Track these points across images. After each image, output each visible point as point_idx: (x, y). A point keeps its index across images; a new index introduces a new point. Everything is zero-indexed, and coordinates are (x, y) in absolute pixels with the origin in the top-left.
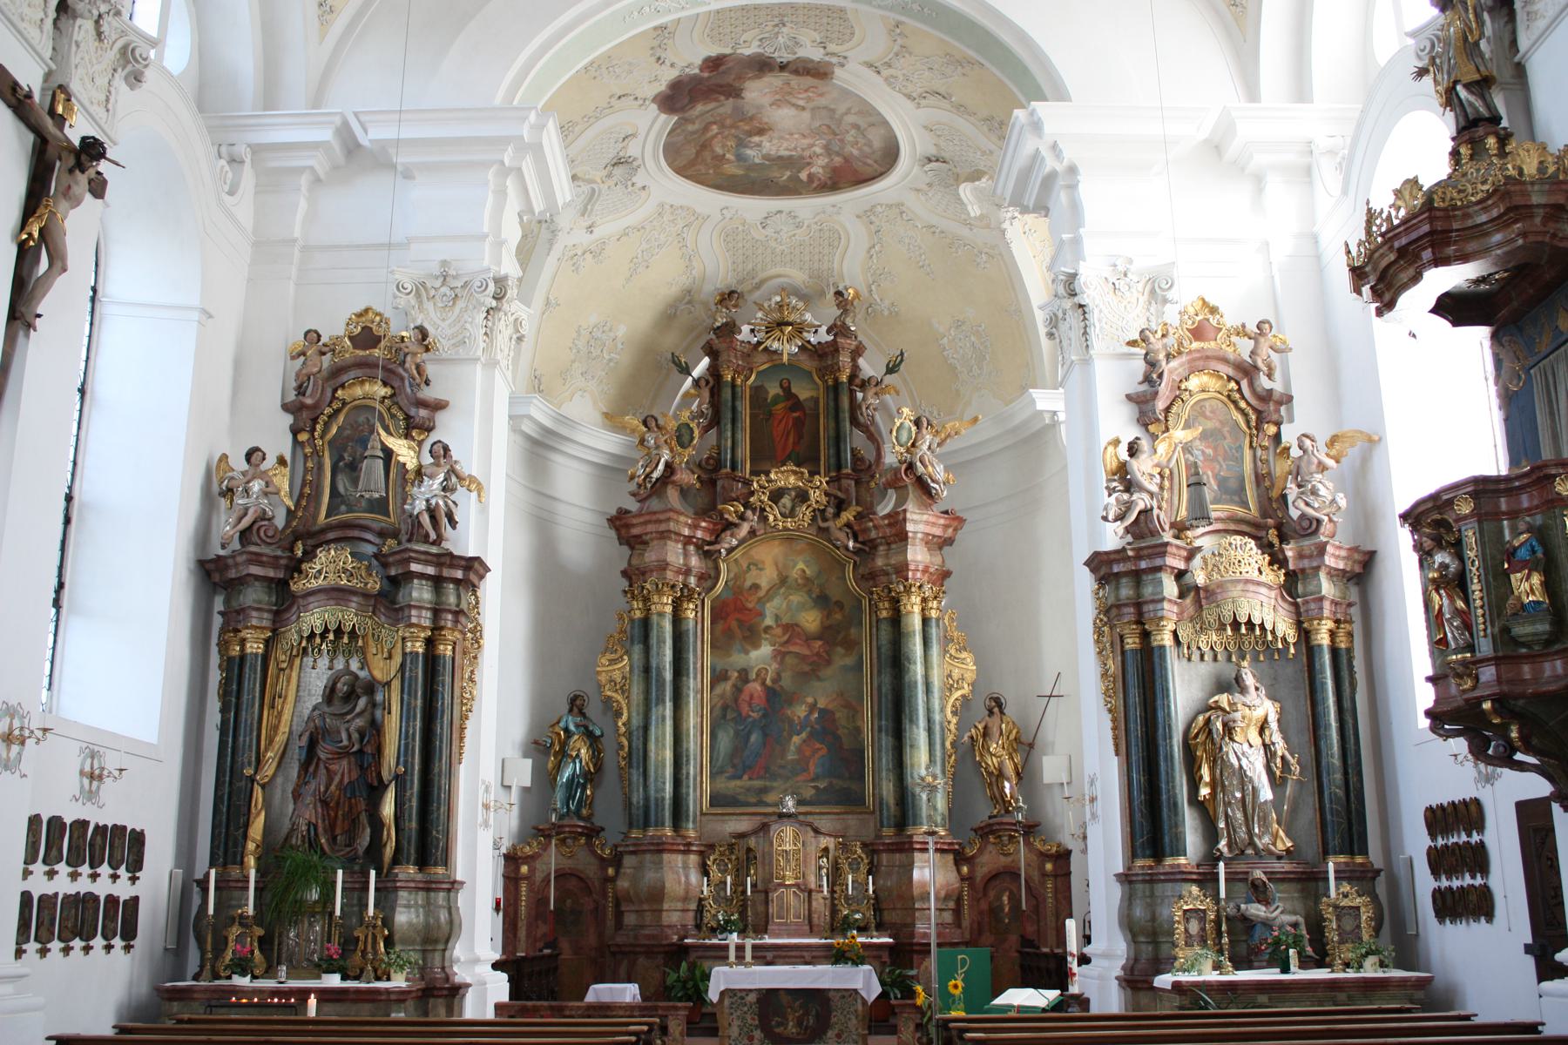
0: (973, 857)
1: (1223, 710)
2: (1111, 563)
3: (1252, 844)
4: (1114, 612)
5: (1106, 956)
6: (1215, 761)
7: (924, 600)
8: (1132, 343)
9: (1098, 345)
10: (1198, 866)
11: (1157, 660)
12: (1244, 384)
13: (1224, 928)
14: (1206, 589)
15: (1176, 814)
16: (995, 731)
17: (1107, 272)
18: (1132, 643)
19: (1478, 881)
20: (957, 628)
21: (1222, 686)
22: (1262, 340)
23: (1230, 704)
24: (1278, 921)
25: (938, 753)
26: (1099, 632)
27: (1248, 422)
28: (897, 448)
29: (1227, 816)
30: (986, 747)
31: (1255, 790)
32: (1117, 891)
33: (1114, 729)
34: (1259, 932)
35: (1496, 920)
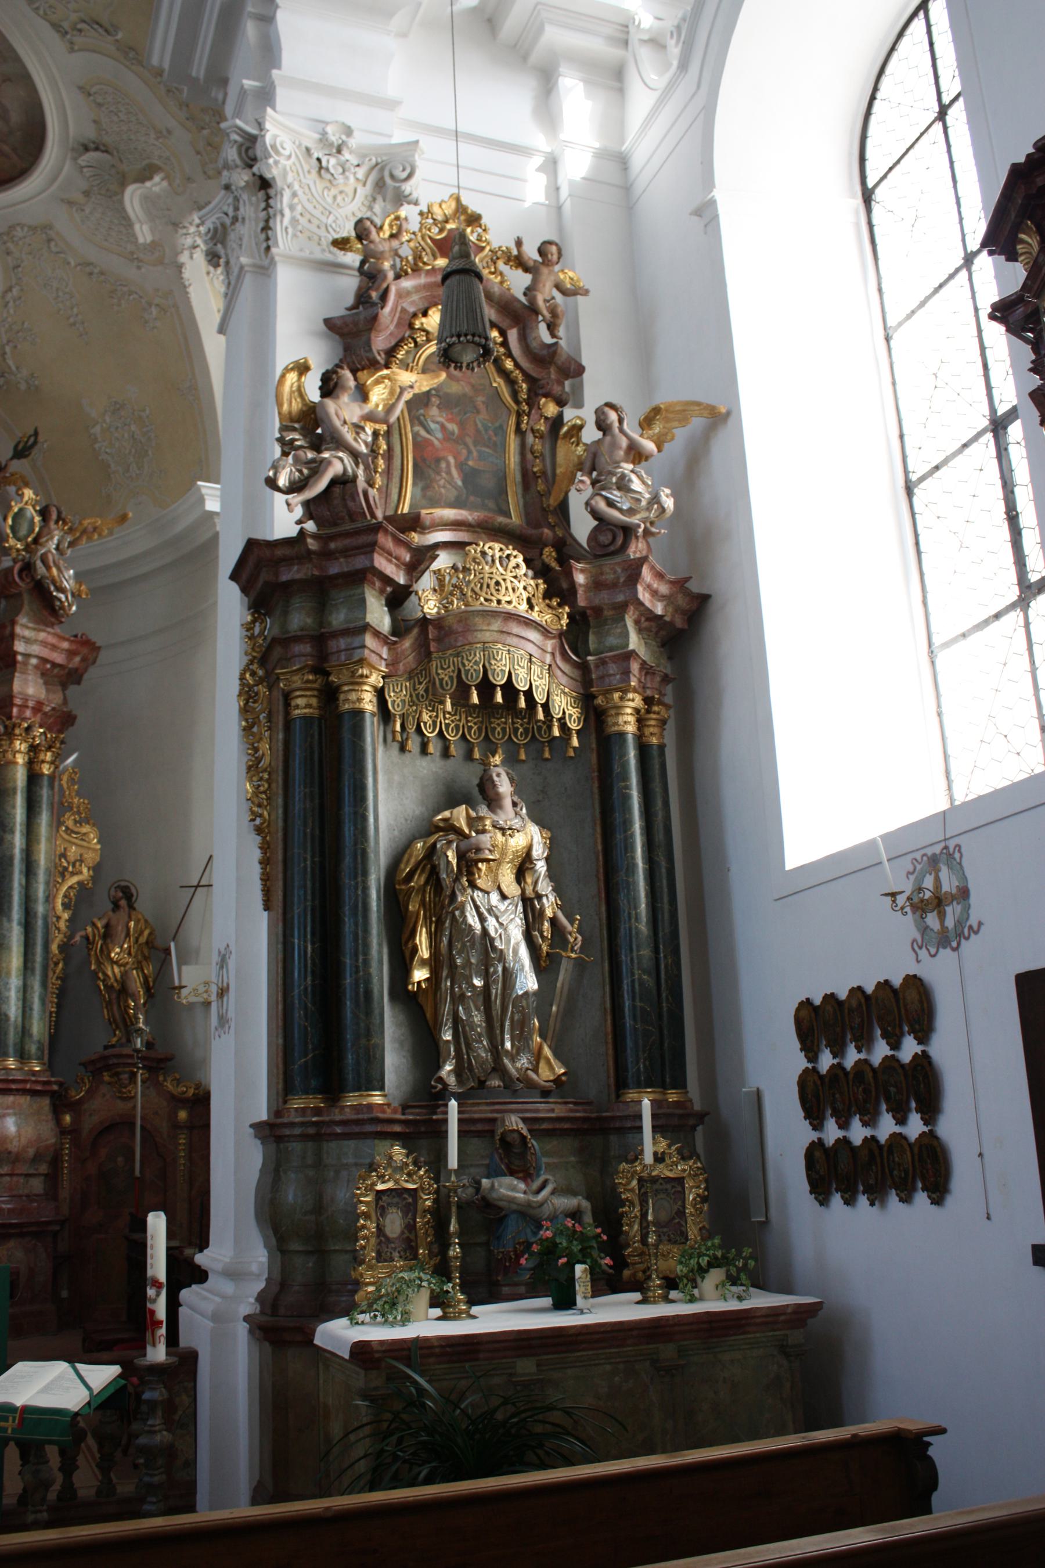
0: (80, 1101)
1: (459, 832)
2: (277, 563)
3: (498, 1069)
4: (278, 652)
5: (233, 1274)
6: (440, 923)
7: (33, 749)
8: (341, 244)
9: (284, 242)
10: (405, 1107)
11: (346, 735)
12: (513, 335)
13: (453, 1227)
14: (438, 622)
15: (369, 1013)
16: (120, 929)
17: (309, 139)
18: (304, 705)
19: (915, 1127)
20: (78, 794)
21: (452, 798)
22: (545, 270)
23: (470, 821)
24: (547, 1210)
25: (39, 958)
26: (247, 694)
27: (515, 394)
28: (12, 542)
29: (456, 1020)
30: (106, 951)
31: (509, 976)
32: (255, 1155)
33: (265, 862)
34: (512, 1231)
35: (950, 1200)
